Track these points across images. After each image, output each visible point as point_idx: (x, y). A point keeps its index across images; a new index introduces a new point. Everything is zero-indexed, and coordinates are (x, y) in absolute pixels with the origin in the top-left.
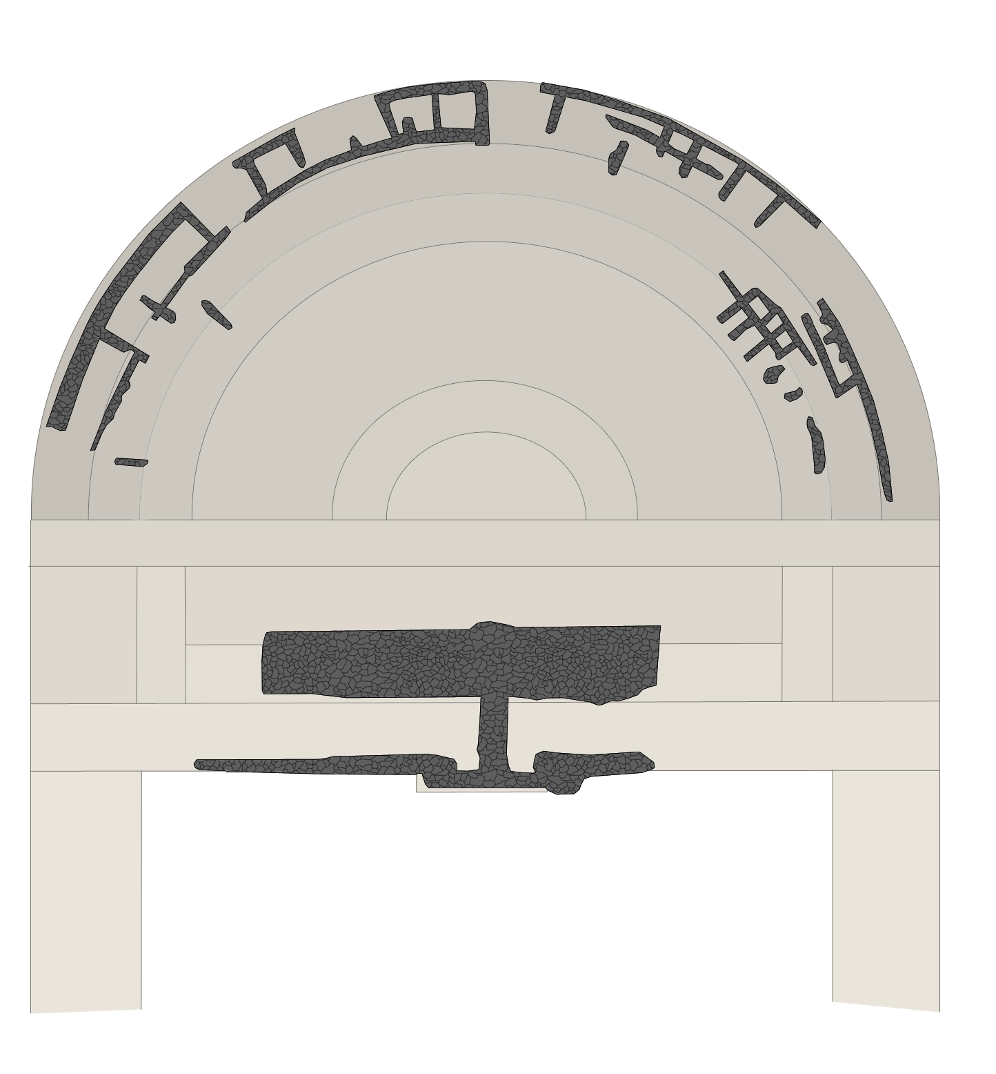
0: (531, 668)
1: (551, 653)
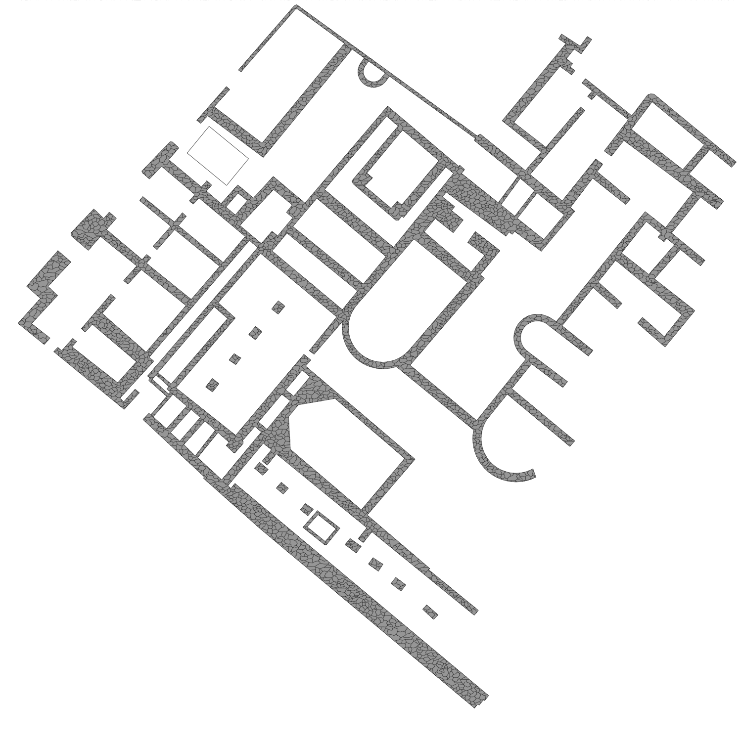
0: (432, 213)
1: (447, 401)
